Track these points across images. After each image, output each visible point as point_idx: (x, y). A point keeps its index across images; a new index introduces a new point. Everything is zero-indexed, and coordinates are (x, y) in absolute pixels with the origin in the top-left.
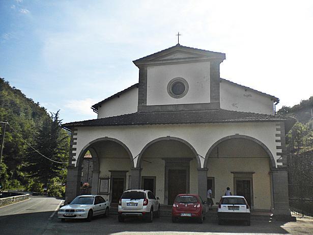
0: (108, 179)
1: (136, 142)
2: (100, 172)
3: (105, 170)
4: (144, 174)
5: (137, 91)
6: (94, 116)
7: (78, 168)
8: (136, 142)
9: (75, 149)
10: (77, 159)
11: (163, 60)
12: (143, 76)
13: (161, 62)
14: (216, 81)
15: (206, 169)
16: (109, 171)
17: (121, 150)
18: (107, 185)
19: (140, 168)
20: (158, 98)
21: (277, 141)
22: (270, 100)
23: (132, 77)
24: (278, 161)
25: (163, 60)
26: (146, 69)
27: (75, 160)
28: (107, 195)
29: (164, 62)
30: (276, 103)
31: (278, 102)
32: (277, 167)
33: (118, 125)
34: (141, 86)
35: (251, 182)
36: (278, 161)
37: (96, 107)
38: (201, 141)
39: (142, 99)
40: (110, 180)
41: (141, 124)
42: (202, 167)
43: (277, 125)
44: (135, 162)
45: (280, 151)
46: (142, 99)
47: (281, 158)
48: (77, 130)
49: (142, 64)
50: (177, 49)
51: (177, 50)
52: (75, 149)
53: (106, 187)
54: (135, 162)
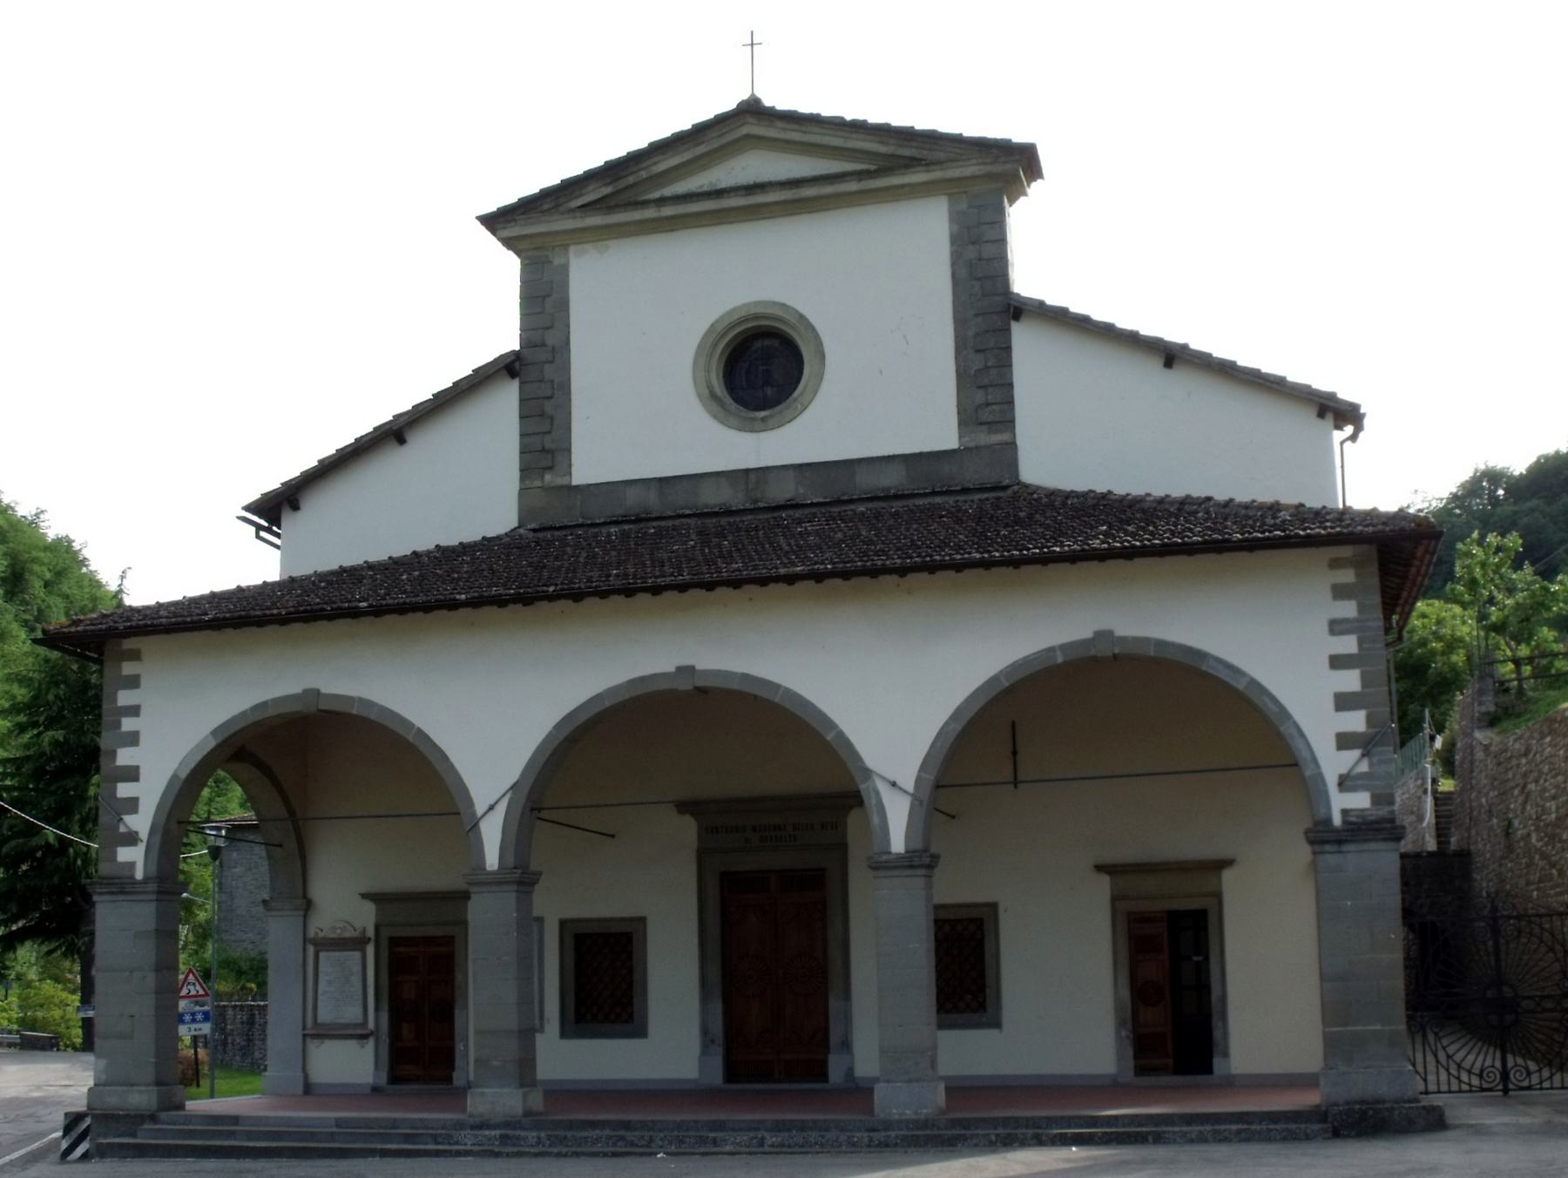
0: (358, 943)
1: (484, 715)
2: (307, 906)
3: (342, 893)
4: (958, 887)
5: (508, 396)
6: (257, 564)
7: (152, 887)
8: (484, 715)
9: (132, 774)
10: (144, 834)
11: (662, 201)
12: (544, 303)
13: (650, 213)
14: (991, 315)
15: (921, 860)
16: (365, 896)
17: (402, 767)
18: (356, 980)
19: (521, 876)
20: (647, 426)
21: (1337, 662)
22: (1313, 412)
23: (484, 313)
24: (1345, 783)
25: (662, 201)
26: (557, 261)
27: (131, 839)
28: (363, 1037)
29: (668, 211)
30: (1349, 429)
31: (1359, 428)
32: (1337, 820)
33: (378, 612)
34: (534, 374)
35: (1212, 919)
36: (1345, 783)
37: (273, 510)
38: (888, 688)
39: (544, 441)
40: (370, 950)
41: (618, 592)
42: (898, 845)
43: (1335, 564)
44: (492, 835)
45: (1356, 721)
46: (544, 441)
47: (1364, 767)
48: (135, 656)
49: (537, 226)
50: (744, 130)
51: (748, 136)
52: (132, 774)
53: (349, 989)
54: (492, 835)
